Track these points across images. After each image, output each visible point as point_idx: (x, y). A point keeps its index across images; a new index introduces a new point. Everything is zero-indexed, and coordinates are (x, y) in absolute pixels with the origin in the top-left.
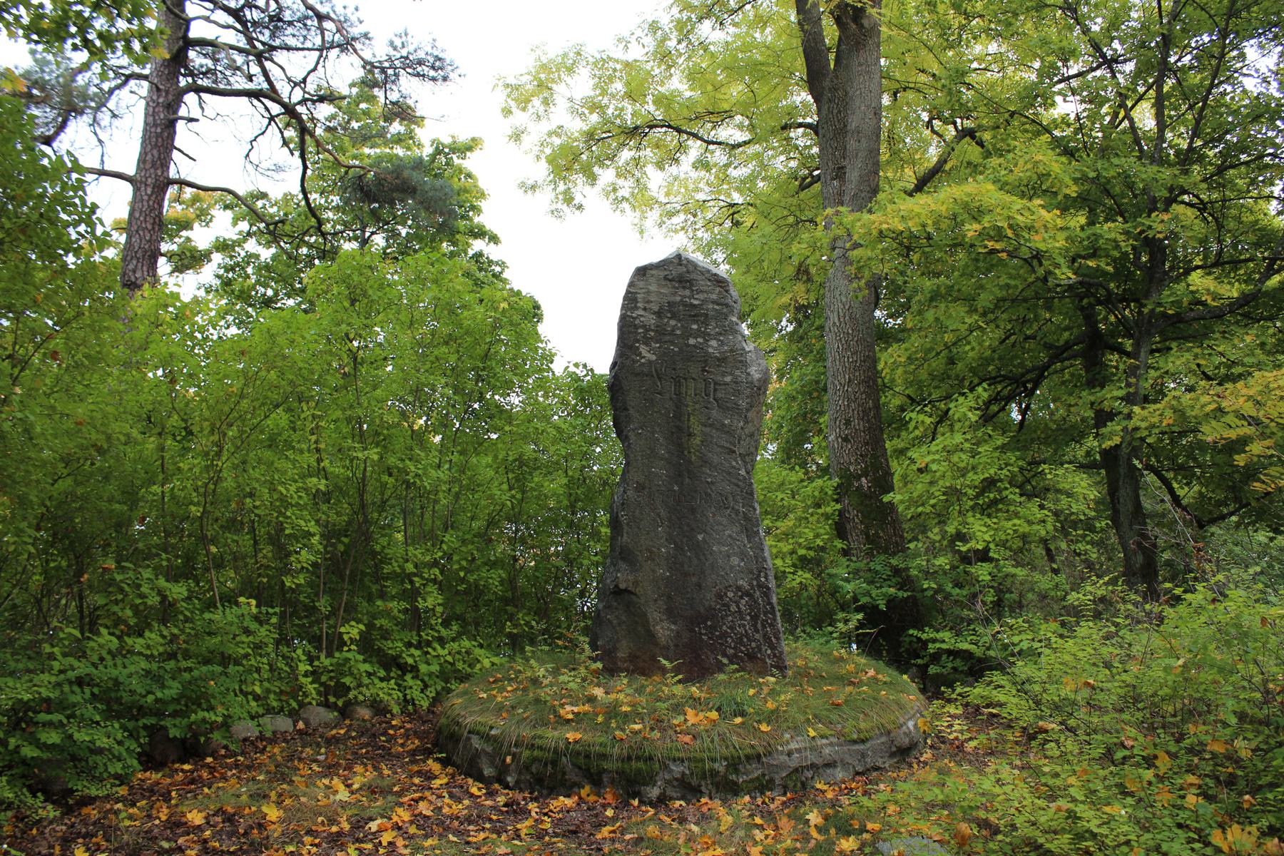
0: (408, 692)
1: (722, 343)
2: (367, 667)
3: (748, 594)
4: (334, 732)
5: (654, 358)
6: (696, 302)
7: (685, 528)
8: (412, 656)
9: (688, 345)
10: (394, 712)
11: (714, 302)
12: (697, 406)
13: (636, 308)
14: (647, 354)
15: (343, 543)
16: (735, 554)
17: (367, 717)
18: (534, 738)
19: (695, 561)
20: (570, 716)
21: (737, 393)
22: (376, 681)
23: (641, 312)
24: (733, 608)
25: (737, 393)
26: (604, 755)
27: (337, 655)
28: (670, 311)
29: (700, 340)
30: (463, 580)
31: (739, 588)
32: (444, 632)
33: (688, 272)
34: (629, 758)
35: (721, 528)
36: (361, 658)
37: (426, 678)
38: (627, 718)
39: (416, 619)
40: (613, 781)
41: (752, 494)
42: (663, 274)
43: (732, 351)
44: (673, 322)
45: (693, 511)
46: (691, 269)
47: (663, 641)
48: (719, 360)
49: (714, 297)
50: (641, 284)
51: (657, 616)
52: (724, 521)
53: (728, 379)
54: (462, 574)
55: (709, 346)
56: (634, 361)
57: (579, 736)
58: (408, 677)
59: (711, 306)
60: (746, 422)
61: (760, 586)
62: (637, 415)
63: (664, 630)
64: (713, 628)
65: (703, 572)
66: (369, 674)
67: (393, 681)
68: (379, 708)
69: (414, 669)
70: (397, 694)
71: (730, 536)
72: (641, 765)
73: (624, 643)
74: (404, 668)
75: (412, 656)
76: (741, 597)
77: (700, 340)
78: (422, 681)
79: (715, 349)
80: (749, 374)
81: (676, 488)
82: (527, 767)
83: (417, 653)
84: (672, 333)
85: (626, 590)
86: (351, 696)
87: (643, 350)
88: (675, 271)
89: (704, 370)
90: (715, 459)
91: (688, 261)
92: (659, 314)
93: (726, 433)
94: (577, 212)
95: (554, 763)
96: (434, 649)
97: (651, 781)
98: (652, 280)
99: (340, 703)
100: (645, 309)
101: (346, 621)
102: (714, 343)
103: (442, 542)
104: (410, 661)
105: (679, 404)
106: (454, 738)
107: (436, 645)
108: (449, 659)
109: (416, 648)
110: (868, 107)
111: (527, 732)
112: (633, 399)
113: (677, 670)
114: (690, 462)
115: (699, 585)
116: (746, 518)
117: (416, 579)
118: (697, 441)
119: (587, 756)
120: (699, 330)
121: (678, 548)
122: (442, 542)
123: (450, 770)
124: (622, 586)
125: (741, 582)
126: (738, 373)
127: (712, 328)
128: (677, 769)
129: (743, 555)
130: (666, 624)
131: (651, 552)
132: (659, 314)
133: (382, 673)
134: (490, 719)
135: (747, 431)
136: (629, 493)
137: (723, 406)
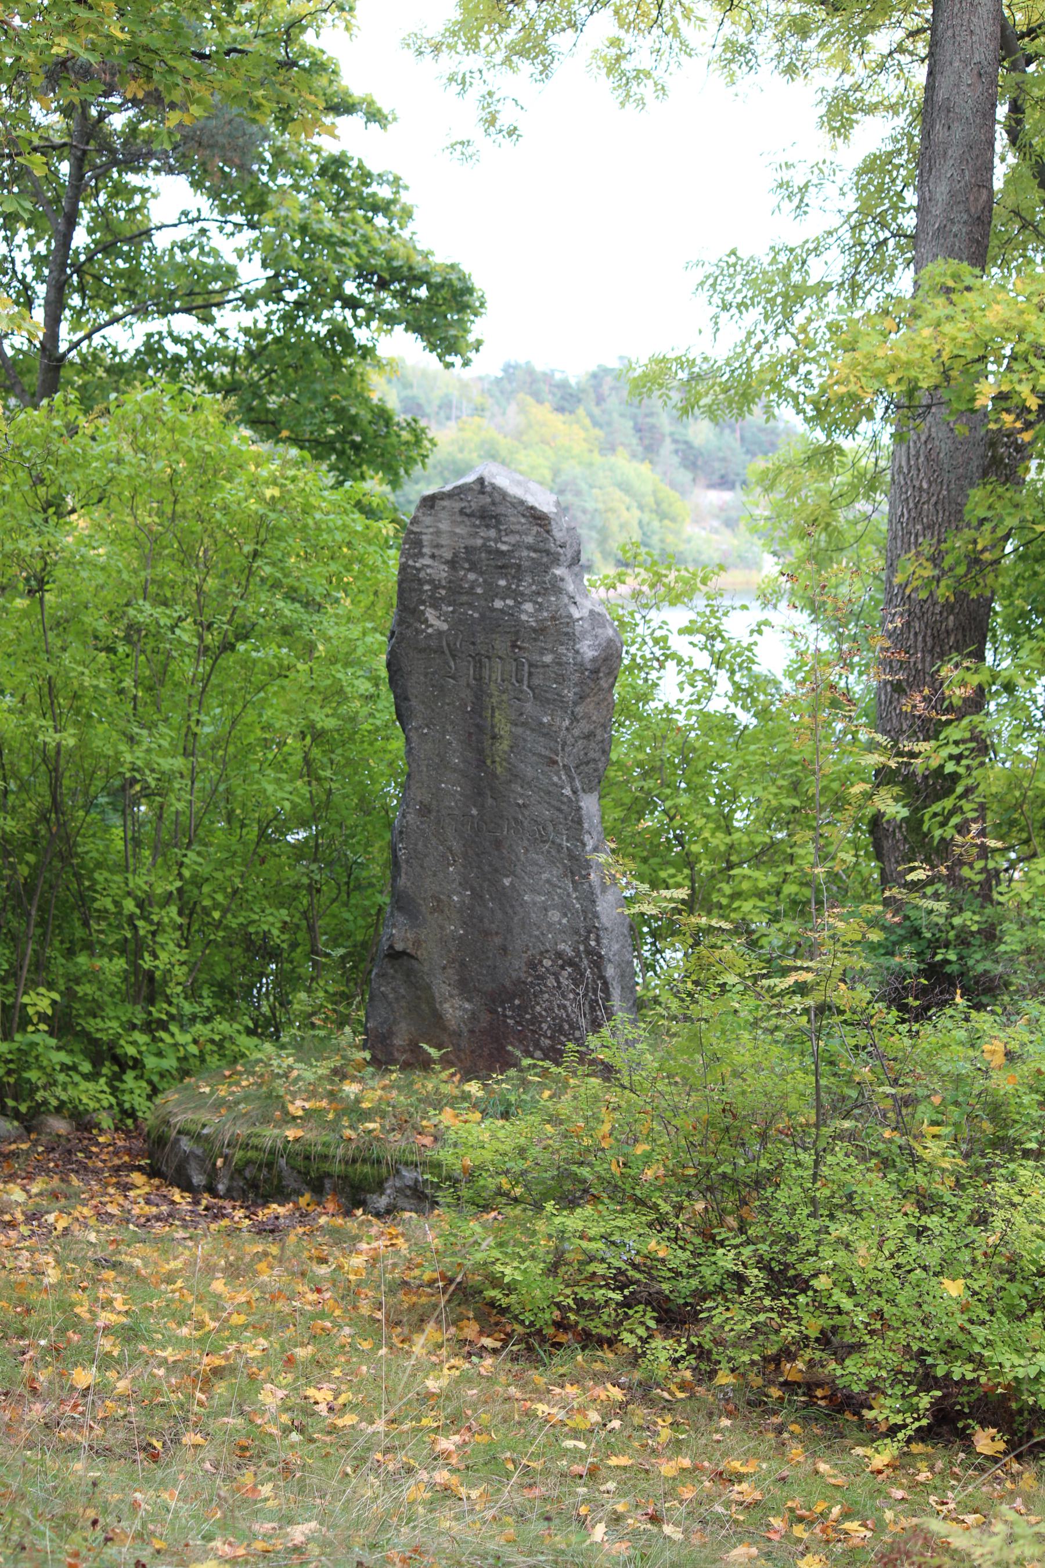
0: (126, 1097)
1: (540, 607)
2: (62, 1057)
3: (571, 963)
4: (13, 1147)
5: (445, 627)
6: (504, 548)
7: (487, 868)
8: (134, 1043)
9: (493, 610)
10: (104, 1126)
11: (530, 548)
12: (505, 697)
13: (421, 555)
14: (435, 621)
15: (27, 863)
16: (554, 907)
17: (62, 1132)
18: (249, 1136)
19: (499, 915)
20: (300, 1113)
21: (561, 679)
22: (77, 1078)
23: (427, 561)
24: (551, 982)
25: (561, 679)
26: (326, 1157)
27: (18, 1037)
28: (467, 560)
29: (510, 602)
30: (218, 925)
31: (559, 955)
32: (188, 1008)
33: (493, 503)
34: (354, 1161)
35: (536, 869)
36: (53, 1042)
37: (155, 1079)
38: (366, 1115)
39: (147, 988)
40: (335, 1191)
41: (580, 822)
42: (458, 505)
43: (553, 618)
44: (471, 576)
45: (498, 844)
46: (498, 498)
47: (453, 1025)
48: (534, 630)
49: (530, 540)
50: (428, 520)
51: (446, 989)
52: (541, 859)
53: (548, 659)
54: (216, 915)
55: (521, 611)
56: (418, 632)
57: (300, 1133)
58: (129, 1076)
59: (525, 553)
60: (574, 719)
61: (589, 952)
62: (422, 708)
63: (455, 1010)
64: (522, 1009)
65: (509, 930)
66: (65, 1068)
67: (103, 1080)
68: (83, 1123)
69: (137, 1064)
70: (108, 1099)
71: (548, 881)
72: (367, 1169)
73: (403, 1025)
74: (123, 1064)
75: (134, 1043)
76: (562, 967)
77: (510, 602)
78: (150, 1082)
79: (530, 615)
80: (577, 652)
81: (474, 812)
82: (239, 1171)
83: (142, 1038)
84: (471, 591)
85: (404, 953)
86: (39, 1097)
87: (430, 614)
88: (475, 503)
89: (514, 646)
90: (529, 772)
91: (494, 487)
92: (453, 564)
93: (545, 735)
94: (507, 142)
95: (270, 1165)
96: (173, 1035)
97: (379, 1187)
98: (443, 515)
99: (23, 1108)
100: (433, 556)
101: (34, 984)
102: (529, 607)
103: (181, 864)
104: (131, 1051)
105: (480, 693)
106: (161, 1141)
107: (174, 1028)
108: (193, 1049)
109: (143, 1031)
110: (966, 62)
111: (242, 1130)
112: (415, 683)
113: (446, 1062)
114: (495, 776)
115: (504, 949)
116: (572, 857)
117: (140, 923)
118: (505, 745)
119: (307, 1158)
120: (508, 587)
121: (477, 896)
122: (181, 864)
123: (156, 1181)
124: (399, 947)
125: (562, 946)
126: (562, 649)
127: (526, 585)
128: (409, 1175)
129: (565, 908)
130: (457, 1002)
131: (439, 901)
132: (453, 564)
133: (86, 1067)
134: (204, 1116)
135: (576, 732)
136: (409, 817)
137: (541, 698)
